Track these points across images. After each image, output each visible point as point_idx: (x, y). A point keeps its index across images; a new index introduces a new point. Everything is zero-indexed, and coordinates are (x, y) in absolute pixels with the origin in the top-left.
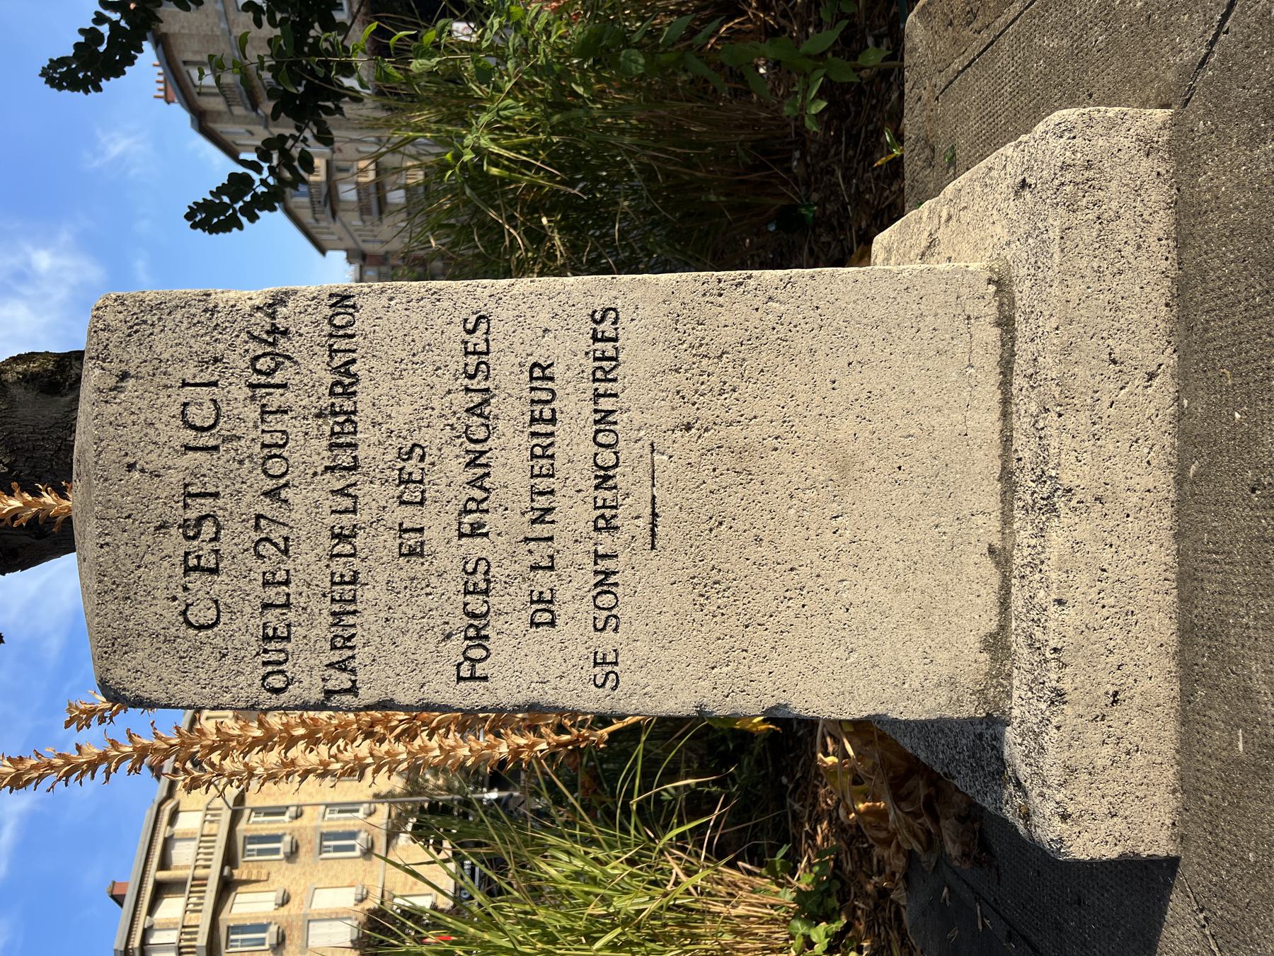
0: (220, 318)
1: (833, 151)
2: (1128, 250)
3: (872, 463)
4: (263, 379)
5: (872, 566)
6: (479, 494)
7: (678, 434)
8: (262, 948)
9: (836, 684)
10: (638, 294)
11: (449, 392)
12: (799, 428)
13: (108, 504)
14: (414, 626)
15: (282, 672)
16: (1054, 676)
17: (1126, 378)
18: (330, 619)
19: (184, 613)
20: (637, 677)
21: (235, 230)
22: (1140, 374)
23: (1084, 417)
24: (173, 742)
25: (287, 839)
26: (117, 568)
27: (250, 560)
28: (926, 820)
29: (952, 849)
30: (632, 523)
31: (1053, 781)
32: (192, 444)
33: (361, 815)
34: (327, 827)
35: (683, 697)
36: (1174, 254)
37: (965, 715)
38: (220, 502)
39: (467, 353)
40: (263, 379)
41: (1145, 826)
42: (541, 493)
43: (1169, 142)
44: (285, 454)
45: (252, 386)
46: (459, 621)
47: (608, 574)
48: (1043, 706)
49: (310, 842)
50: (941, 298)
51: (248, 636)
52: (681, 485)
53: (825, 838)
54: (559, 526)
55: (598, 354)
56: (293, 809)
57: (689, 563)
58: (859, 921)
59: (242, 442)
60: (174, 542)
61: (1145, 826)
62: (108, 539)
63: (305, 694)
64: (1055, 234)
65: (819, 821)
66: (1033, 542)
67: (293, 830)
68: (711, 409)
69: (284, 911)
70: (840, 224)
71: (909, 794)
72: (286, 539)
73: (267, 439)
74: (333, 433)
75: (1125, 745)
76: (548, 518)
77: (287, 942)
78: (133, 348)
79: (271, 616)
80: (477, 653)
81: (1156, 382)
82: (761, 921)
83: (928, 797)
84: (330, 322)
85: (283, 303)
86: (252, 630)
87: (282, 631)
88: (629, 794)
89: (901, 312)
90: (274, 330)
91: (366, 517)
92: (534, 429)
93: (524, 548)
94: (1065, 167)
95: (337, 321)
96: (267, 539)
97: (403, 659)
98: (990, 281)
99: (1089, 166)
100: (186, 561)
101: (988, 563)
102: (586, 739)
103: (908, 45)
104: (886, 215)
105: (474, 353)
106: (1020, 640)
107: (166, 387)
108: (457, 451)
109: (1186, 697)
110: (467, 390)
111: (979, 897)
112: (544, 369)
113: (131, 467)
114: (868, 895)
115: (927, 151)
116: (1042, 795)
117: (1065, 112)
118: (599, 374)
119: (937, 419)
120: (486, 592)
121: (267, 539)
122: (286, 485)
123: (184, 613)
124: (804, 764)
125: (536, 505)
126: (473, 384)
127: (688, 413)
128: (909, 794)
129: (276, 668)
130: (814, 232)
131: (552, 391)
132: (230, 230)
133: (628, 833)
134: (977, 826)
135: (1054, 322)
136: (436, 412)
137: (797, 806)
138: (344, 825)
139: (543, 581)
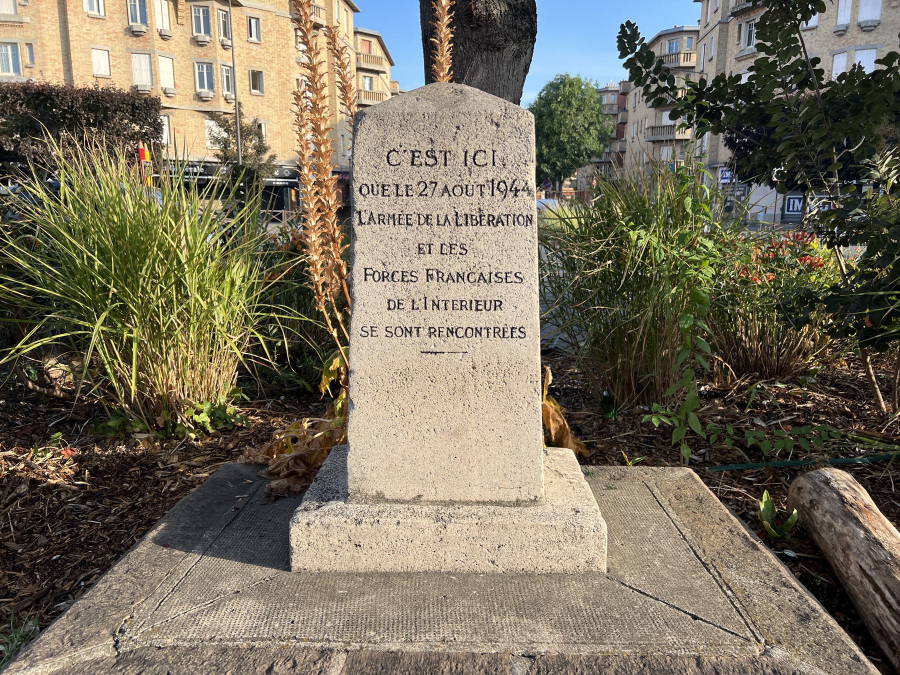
0: (523, 167)
1: (645, 429)
2: (546, 553)
3: (458, 446)
4: (495, 186)
5: (413, 445)
6: (445, 278)
7: (471, 364)
8: (130, 21)
9: (363, 430)
10: (532, 347)
11: (490, 266)
12: (473, 415)
13: (442, 118)
14: (388, 250)
15: (369, 193)
16: (367, 520)
17: (492, 552)
18: (392, 214)
19: (394, 150)
20: (366, 345)
21: (619, 53)
22: (494, 557)
23: (476, 534)
24: (318, 84)
25: (208, 39)
26: (414, 122)
27: (418, 179)
28: (285, 472)
29: (274, 484)
30: (433, 343)
31: (323, 520)
32: (468, 155)
33: (226, 92)
34: (217, 68)
35: (357, 364)
36: (544, 572)
37: (349, 485)
38: (442, 167)
39: (506, 273)
40: (495, 186)
41: (304, 557)
42: (445, 304)
43: (592, 571)
44: (463, 195)
45: (493, 181)
46: (390, 270)
47: (410, 333)
48: (354, 516)
49: (205, 55)
50: (529, 476)
51: (384, 178)
52: (449, 364)
53: (253, 421)
54: (432, 313)
55: (506, 330)
56: (229, 43)
57: (415, 367)
58: (212, 439)
59: (468, 176)
60: (425, 146)
61: (304, 557)
62: (427, 118)
63: (359, 203)
64: (553, 523)
65: (263, 417)
66: (424, 513)
67: (213, 43)
68: (482, 378)
69: (156, 36)
70: (602, 433)
71: (297, 464)
72: (426, 195)
73: (470, 187)
74: (472, 216)
75: (339, 549)
76: (435, 307)
77: (135, 39)
78: (510, 129)
79: (393, 188)
80: (377, 276)
81: (490, 564)
82: (209, 384)
83: (298, 473)
84: (520, 215)
85: (529, 194)
86: (387, 180)
87: (386, 193)
88: (277, 311)
89: (523, 459)
90: (517, 190)
91: (435, 229)
92: (474, 302)
93: (422, 297)
94: (582, 527)
95: (521, 218)
96: (426, 187)
97: (375, 245)
98: (536, 497)
99: (582, 537)
100: (417, 151)
101: (414, 495)
102: (320, 300)
103: (675, 469)
104: (601, 458)
105: (506, 277)
106: (382, 508)
107: (493, 143)
108: (464, 269)
109: (359, 574)
110: (491, 273)
111: (251, 496)
112: (499, 306)
113: (458, 128)
114: (226, 445)
115: (618, 477)
116: (317, 515)
117: (606, 528)
118: (497, 330)
119: (476, 473)
120: (403, 280)
121: (426, 187)
122: (450, 195)
123: (394, 150)
124: (294, 410)
125: (440, 302)
126: (493, 276)
127: (480, 368)
128: (297, 464)
129: (370, 190)
130: (601, 418)
131: (490, 310)
132: (619, 50)
133: (256, 312)
134: (286, 495)
135: (516, 522)
136: (481, 260)
137: (269, 405)
138: (218, 80)
139: (408, 305)
